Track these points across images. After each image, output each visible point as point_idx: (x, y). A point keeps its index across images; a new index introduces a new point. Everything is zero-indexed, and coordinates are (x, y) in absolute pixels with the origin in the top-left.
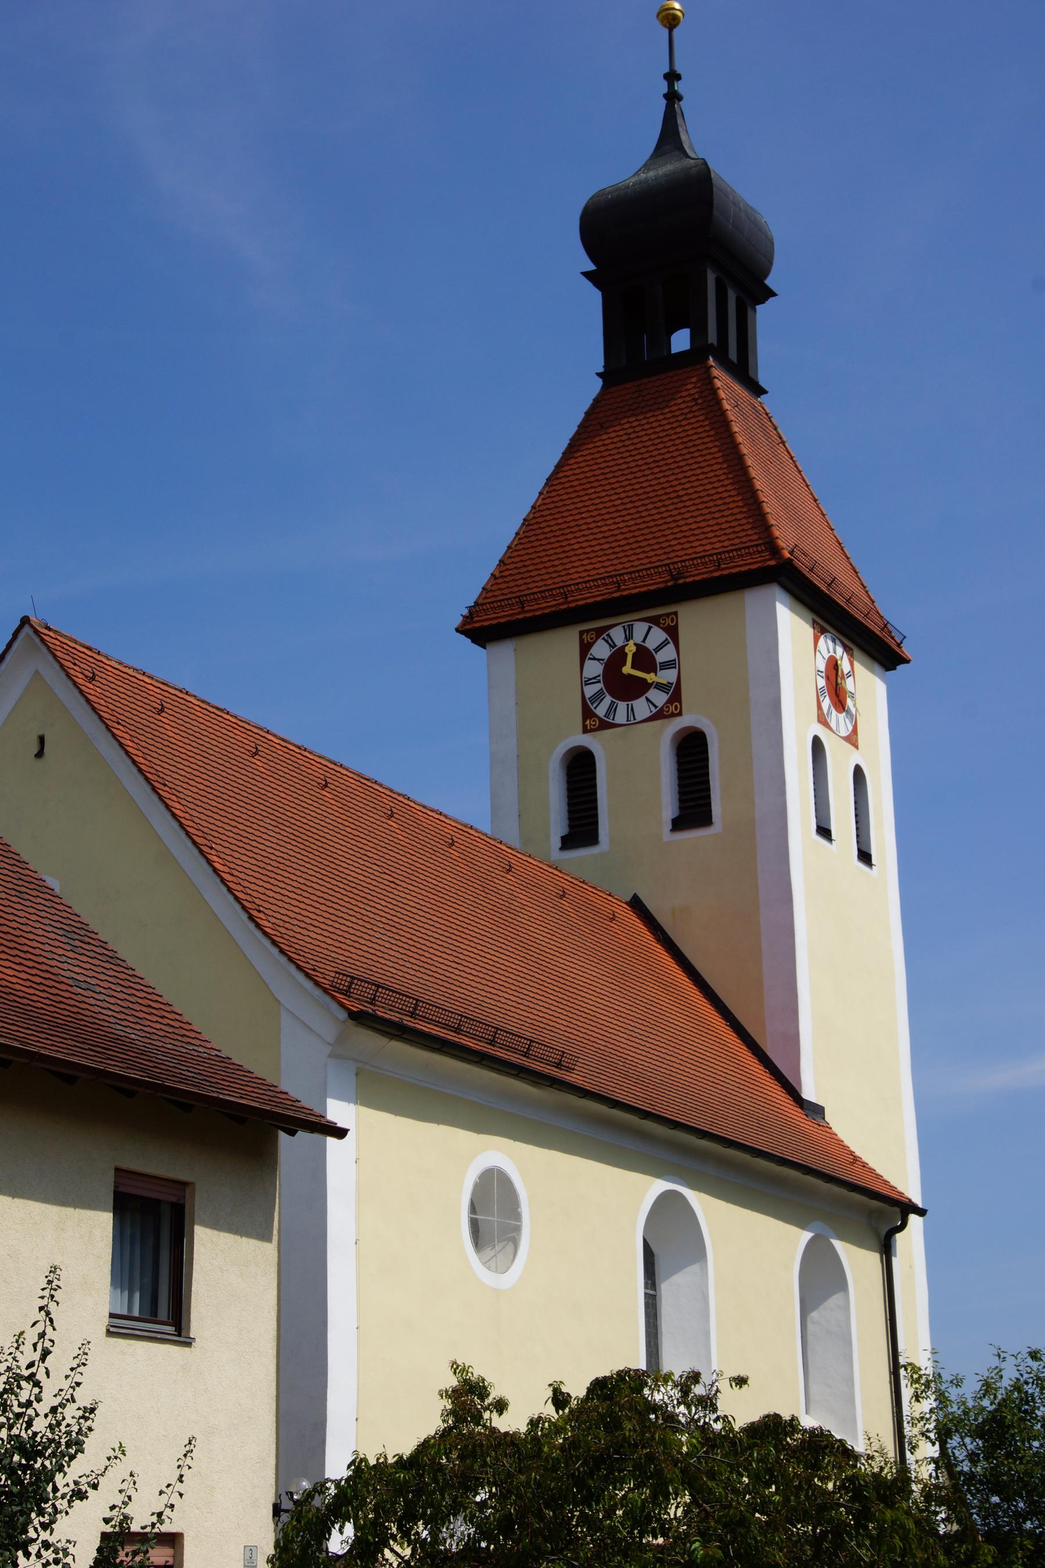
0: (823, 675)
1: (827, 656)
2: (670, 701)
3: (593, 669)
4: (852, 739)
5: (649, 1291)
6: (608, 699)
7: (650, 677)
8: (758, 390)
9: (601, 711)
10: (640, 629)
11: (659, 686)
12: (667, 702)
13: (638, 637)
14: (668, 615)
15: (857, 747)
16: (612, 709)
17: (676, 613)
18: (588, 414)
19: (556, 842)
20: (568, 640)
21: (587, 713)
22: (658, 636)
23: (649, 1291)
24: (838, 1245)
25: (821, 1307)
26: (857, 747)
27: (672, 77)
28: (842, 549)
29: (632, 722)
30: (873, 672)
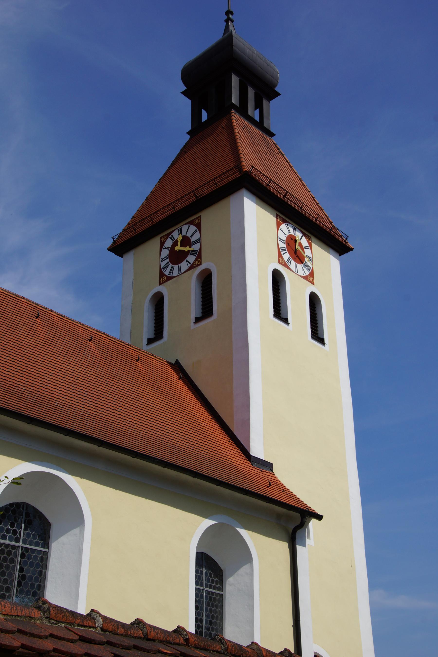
0: (285, 242)
1: (288, 234)
2: (196, 259)
3: (165, 253)
4: (310, 278)
5: (198, 587)
6: (171, 265)
7: (187, 249)
8: (271, 135)
9: (167, 273)
10: (185, 228)
11: (193, 253)
12: (195, 260)
13: (184, 233)
14: (197, 218)
15: (313, 284)
17: (200, 216)
18: (181, 150)
19: (145, 342)
20: (155, 242)
21: (162, 275)
22: (193, 228)
23: (198, 587)
24: (244, 533)
25: (235, 575)
26: (313, 284)
27: (228, 13)
28: (314, 199)
29: (180, 273)
30: (329, 253)
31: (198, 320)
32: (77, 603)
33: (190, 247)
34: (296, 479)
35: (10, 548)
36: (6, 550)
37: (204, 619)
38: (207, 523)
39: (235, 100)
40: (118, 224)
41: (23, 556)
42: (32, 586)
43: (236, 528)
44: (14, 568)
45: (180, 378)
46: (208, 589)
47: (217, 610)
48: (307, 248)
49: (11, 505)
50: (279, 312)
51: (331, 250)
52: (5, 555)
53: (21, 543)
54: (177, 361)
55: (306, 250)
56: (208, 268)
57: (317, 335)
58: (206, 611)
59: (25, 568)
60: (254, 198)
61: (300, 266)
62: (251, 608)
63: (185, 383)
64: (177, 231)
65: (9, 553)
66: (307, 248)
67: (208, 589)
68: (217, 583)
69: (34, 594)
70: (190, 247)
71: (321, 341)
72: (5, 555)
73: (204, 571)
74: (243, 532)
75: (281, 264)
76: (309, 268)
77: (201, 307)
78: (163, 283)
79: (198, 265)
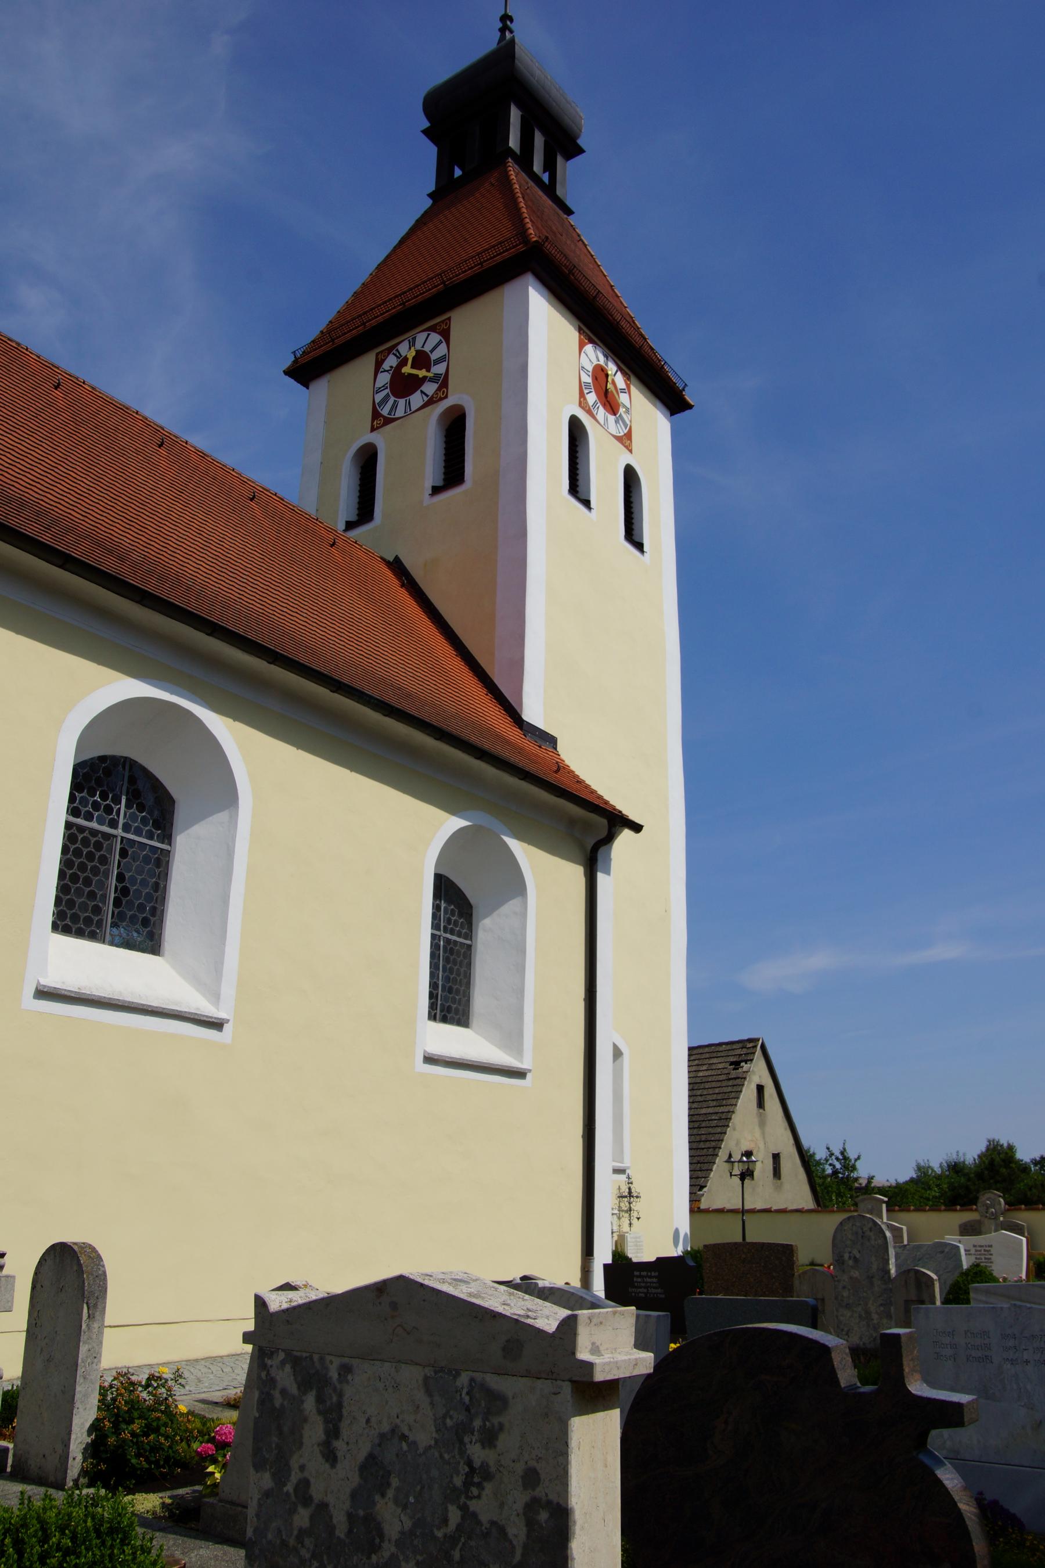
1: (595, 362)
2: (439, 389)
3: (384, 378)
4: (626, 440)
6: (392, 399)
7: (422, 373)
8: (569, 212)
9: (385, 411)
10: (421, 338)
11: (434, 379)
13: (418, 345)
14: (442, 322)
15: (631, 451)
16: (395, 406)
17: (449, 319)
20: (368, 360)
21: (376, 414)
22: (435, 338)
26: (631, 451)
29: (409, 412)
30: (655, 405)
31: (436, 490)
32: (224, 944)
33: (428, 371)
34: (593, 759)
35: (99, 838)
36: (93, 840)
37: (440, 983)
38: (456, 823)
39: (514, 142)
40: (307, 331)
41: (123, 853)
42: (141, 908)
43: (506, 839)
44: (106, 874)
45: (402, 586)
46: (448, 936)
47: (462, 970)
48: (623, 391)
49: (103, 759)
50: (578, 487)
51: (659, 404)
52: (91, 849)
53: (120, 831)
54: (397, 558)
55: (621, 395)
56: (459, 403)
57: (633, 535)
58: (444, 971)
59: (127, 875)
60: (546, 292)
61: (611, 418)
62: (520, 969)
63: (411, 594)
64: (407, 342)
65: (98, 846)
66: (623, 391)
67: (448, 936)
68: (462, 927)
69: (145, 922)
70: (428, 371)
71: (639, 546)
72: (91, 849)
73: (443, 905)
74: (514, 845)
75: (583, 408)
76: (626, 425)
77: (443, 470)
78: (378, 428)
79: (441, 399)
